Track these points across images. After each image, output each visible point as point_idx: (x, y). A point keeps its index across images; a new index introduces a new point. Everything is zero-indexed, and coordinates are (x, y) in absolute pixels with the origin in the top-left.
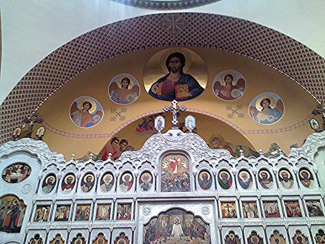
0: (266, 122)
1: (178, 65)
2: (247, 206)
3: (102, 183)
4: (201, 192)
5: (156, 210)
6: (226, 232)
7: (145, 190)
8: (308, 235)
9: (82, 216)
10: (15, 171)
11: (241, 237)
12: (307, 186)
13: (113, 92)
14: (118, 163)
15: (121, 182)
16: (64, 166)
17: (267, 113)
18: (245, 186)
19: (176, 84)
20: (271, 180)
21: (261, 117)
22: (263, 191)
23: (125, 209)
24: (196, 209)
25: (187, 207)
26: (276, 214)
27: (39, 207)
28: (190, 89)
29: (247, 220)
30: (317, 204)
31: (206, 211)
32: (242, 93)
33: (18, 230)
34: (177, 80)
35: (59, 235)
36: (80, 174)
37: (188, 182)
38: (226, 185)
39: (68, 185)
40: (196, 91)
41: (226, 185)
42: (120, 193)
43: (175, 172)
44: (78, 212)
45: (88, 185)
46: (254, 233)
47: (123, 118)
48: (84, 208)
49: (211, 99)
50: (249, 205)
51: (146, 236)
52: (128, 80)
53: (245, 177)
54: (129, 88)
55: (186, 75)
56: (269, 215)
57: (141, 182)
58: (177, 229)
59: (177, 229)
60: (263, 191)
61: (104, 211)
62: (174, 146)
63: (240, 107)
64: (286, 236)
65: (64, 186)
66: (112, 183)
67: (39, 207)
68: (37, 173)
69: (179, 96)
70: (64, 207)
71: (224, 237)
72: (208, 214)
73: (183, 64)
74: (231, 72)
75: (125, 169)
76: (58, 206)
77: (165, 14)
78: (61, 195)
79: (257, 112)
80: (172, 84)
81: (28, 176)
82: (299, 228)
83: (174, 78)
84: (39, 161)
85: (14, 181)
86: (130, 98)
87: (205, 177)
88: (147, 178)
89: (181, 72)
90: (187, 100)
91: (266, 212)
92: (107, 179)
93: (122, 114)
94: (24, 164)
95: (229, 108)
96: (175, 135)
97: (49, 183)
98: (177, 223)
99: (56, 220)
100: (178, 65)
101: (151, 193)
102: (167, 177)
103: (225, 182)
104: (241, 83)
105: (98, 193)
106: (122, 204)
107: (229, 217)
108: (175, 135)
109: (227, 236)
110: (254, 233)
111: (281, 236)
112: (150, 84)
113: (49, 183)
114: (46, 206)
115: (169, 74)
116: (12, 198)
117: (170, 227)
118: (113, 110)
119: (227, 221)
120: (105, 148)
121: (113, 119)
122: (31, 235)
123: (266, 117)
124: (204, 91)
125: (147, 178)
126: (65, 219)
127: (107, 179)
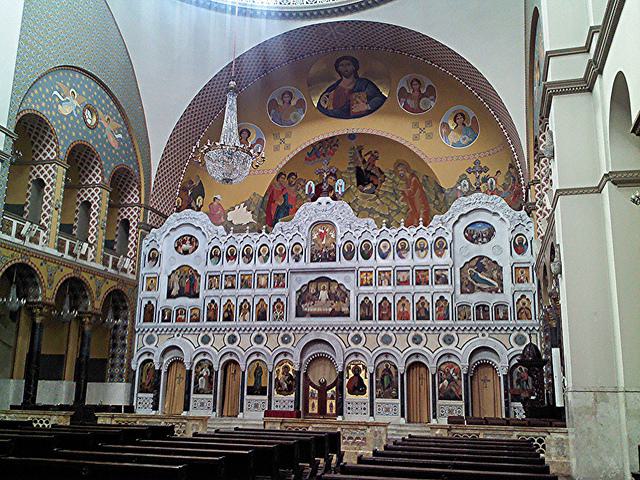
0: (459, 144)
1: (351, 68)
2: (383, 275)
3: (260, 254)
4: (345, 263)
5: (307, 279)
6: (361, 299)
7: (297, 261)
8: (430, 301)
9: (246, 284)
10: (184, 242)
11: (373, 302)
12: (440, 256)
13: (273, 111)
14: (272, 236)
15: (276, 254)
16: (225, 239)
17: (460, 132)
18: (384, 257)
19: (352, 92)
20: (408, 250)
21: (453, 137)
22: (399, 262)
23: (280, 280)
24: (338, 278)
25: (332, 276)
26: (406, 283)
27: (210, 277)
28: (369, 98)
29: (381, 288)
30: (445, 273)
31: (348, 280)
32: (433, 104)
33: (197, 296)
34: (351, 87)
35: (229, 300)
36: (240, 247)
37: (334, 251)
38: (366, 257)
39: (231, 257)
40: (376, 103)
41: (366, 257)
42: (275, 265)
43: (324, 242)
44: (242, 281)
45: (248, 256)
46: (385, 298)
47: (288, 147)
48: (247, 277)
49: (394, 113)
50: (384, 276)
51: (298, 301)
52: (290, 94)
53: (385, 247)
54: (293, 103)
55: (362, 79)
56: (400, 283)
57: (292, 253)
58: (323, 295)
59: (323, 295)
60: (399, 262)
61: (263, 281)
62: (323, 217)
63: (429, 123)
64: (411, 301)
65: (228, 258)
66: (268, 254)
67: (210, 277)
68: (204, 247)
69: (355, 110)
70: (231, 277)
71: (360, 302)
72: (349, 282)
73: (357, 68)
74: (419, 76)
75: (278, 241)
76: (226, 276)
77: (320, 24)
78: (228, 267)
79: (449, 130)
80: (346, 92)
81: (196, 247)
82: (443, 295)
83: (347, 84)
84: (203, 233)
85: (186, 252)
86: (295, 117)
87: (350, 248)
88: (297, 250)
89: (356, 77)
90: (363, 116)
91: (398, 280)
92: (264, 251)
93: (287, 141)
94: (192, 237)
95: (416, 125)
96: (324, 204)
97: (215, 256)
98: (324, 289)
99: (226, 288)
100: (351, 68)
101: (301, 264)
102: (316, 248)
103: (366, 253)
104: (431, 91)
105: (257, 265)
106: (278, 275)
107: (367, 285)
108: (324, 204)
109: (363, 302)
110: (385, 298)
111: (528, 299)
112: (318, 94)
113: (215, 256)
114: (217, 276)
115: (341, 80)
116: (187, 268)
117: (318, 292)
118: (276, 136)
119: (363, 288)
120: (271, 186)
121: (276, 148)
122: (208, 301)
123: (460, 138)
124: (386, 102)
125: (297, 250)
126: (233, 287)
127: (264, 251)
